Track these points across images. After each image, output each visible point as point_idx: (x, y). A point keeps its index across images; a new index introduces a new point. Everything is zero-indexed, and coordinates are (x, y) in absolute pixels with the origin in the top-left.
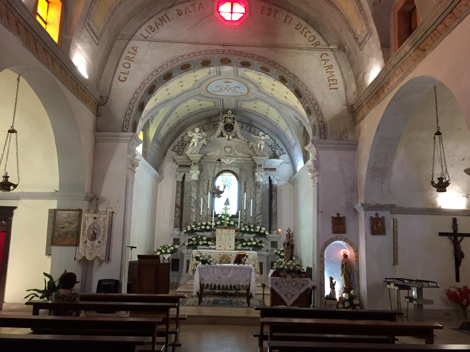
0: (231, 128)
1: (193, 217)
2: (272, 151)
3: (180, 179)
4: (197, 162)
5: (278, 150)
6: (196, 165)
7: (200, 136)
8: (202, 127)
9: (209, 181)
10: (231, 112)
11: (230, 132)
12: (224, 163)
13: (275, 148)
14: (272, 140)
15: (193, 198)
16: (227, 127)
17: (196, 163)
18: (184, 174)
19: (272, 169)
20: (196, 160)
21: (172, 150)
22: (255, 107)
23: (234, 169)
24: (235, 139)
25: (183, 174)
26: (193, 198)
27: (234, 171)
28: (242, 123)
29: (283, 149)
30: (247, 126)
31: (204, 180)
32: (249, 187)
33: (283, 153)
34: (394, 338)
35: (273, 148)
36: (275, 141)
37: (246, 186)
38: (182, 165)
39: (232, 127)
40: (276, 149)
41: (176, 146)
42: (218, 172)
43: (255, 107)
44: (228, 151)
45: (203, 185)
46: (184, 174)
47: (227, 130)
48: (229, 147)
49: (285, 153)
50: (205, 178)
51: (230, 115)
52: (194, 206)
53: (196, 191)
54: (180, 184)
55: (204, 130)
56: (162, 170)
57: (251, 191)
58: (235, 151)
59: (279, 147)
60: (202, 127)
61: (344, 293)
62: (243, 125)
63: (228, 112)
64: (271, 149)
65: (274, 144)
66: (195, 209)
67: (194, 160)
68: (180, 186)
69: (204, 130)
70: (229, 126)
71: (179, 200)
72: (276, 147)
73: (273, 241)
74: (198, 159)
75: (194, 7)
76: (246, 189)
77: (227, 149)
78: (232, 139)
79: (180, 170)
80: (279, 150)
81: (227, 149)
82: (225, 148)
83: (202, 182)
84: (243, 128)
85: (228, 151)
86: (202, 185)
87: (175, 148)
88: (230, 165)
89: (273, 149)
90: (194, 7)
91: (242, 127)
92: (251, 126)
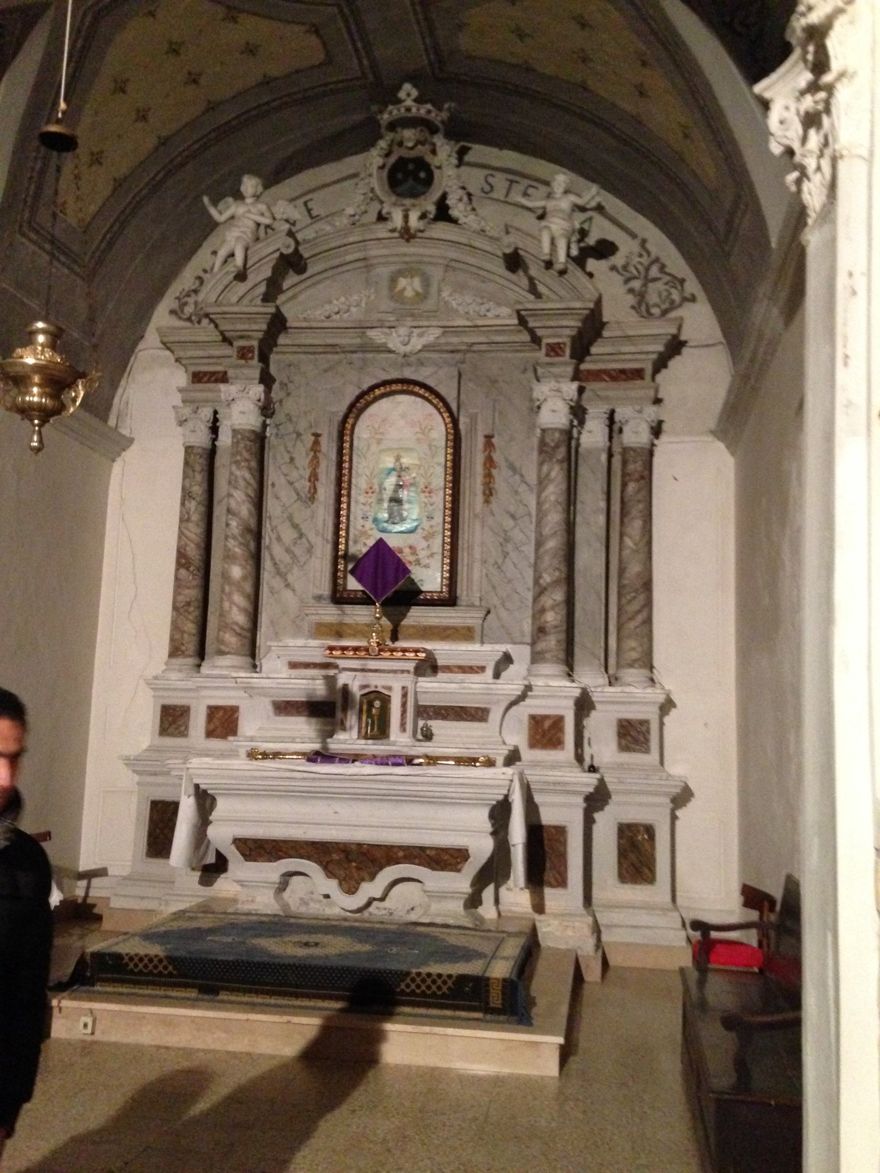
0: (417, 179)
1: (232, 603)
2: (631, 291)
3: (202, 438)
4: (255, 343)
5: (660, 285)
6: (252, 358)
7: (262, 214)
8: (305, 203)
9: (317, 435)
10: (415, 93)
11: (414, 195)
12: (390, 351)
13: (646, 277)
14: (629, 238)
15: (234, 514)
16: (400, 176)
17: (250, 349)
18: (216, 413)
19: (623, 371)
20: (248, 338)
21: (173, 312)
22: (521, 35)
23: (436, 372)
24: (441, 230)
25: (206, 413)
26: (234, 514)
27: (430, 382)
28: (487, 172)
29: (682, 281)
30: (512, 182)
31: (299, 435)
32: (506, 460)
33: (685, 299)
34: (198, 198)
35: (634, 278)
36: (644, 242)
37: (497, 456)
38: (205, 373)
39: (422, 175)
40: (648, 280)
41: (188, 295)
42: (357, 392)
43: (521, 35)
44: (409, 293)
45: (292, 459)
46: (216, 413)
47: (399, 190)
48: (408, 271)
49: (693, 299)
50: (302, 425)
51: (408, 110)
52: (237, 550)
53: (252, 481)
54: (200, 463)
55: (314, 213)
56: (127, 403)
57: (517, 477)
58: (440, 290)
59: (662, 268)
60: (302, 201)
61: (296, 251)
62: (490, 180)
63: (402, 95)
64: (627, 281)
65: (641, 256)
66: (244, 568)
67: (242, 337)
68: (198, 468)
69: (314, 213)
70: (411, 167)
71: (195, 531)
72: (647, 269)
73: (629, 722)
74: (255, 327)
75: (510, 186)
76: (494, 472)
77: (402, 282)
78: (421, 225)
79: (199, 395)
80: (666, 284)
81: (402, 282)
82: (393, 280)
83: (290, 445)
84: (494, 195)
85: (409, 293)
86: (287, 458)
87: (186, 304)
88: (418, 358)
89: (636, 284)
90: (510, 186)
91: (487, 188)
92: (526, 182)
